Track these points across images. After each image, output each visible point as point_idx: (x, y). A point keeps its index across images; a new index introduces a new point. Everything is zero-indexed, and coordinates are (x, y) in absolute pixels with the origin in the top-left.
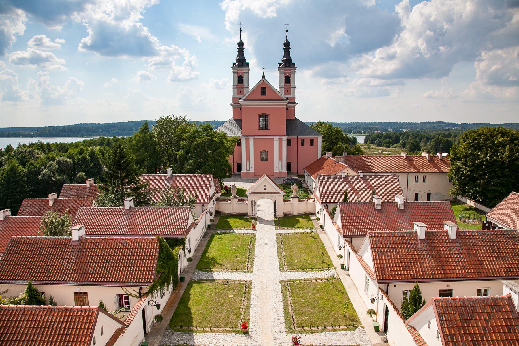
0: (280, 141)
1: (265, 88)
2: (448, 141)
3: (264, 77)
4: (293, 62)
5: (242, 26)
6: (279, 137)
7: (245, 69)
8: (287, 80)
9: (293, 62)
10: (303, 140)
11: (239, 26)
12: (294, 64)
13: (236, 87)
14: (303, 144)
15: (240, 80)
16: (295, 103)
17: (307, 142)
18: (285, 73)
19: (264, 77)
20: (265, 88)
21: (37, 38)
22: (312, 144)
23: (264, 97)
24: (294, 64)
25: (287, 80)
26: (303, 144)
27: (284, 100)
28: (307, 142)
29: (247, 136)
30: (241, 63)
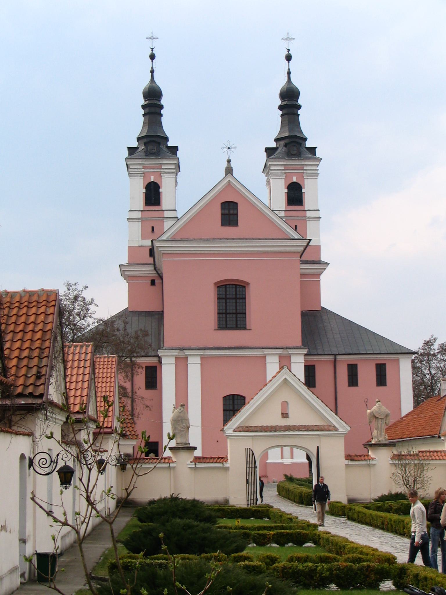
0: (181, 423)
1: (235, 204)
2: (61, 468)
3: (229, 171)
4: (309, 144)
5: (155, 44)
6: (280, 352)
7: (167, 164)
8: (295, 195)
9: (309, 144)
10: (353, 370)
11: (149, 44)
12: (312, 150)
13: (138, 215)
14: (353, 381)
15: (153, 195)
16: (318, 262)
17: (367, 374)
18: (287, 176)
19: (229, 171)
20: (235, 204)
21: (235, 557)
22: (381, 379)
23: (230, 231)
24: (312, 150)
25: (295, 195)
26: (353, 381)
27: (293, 239)
28: (367, 374)
29: (182, 349)
30: (154, 144)
